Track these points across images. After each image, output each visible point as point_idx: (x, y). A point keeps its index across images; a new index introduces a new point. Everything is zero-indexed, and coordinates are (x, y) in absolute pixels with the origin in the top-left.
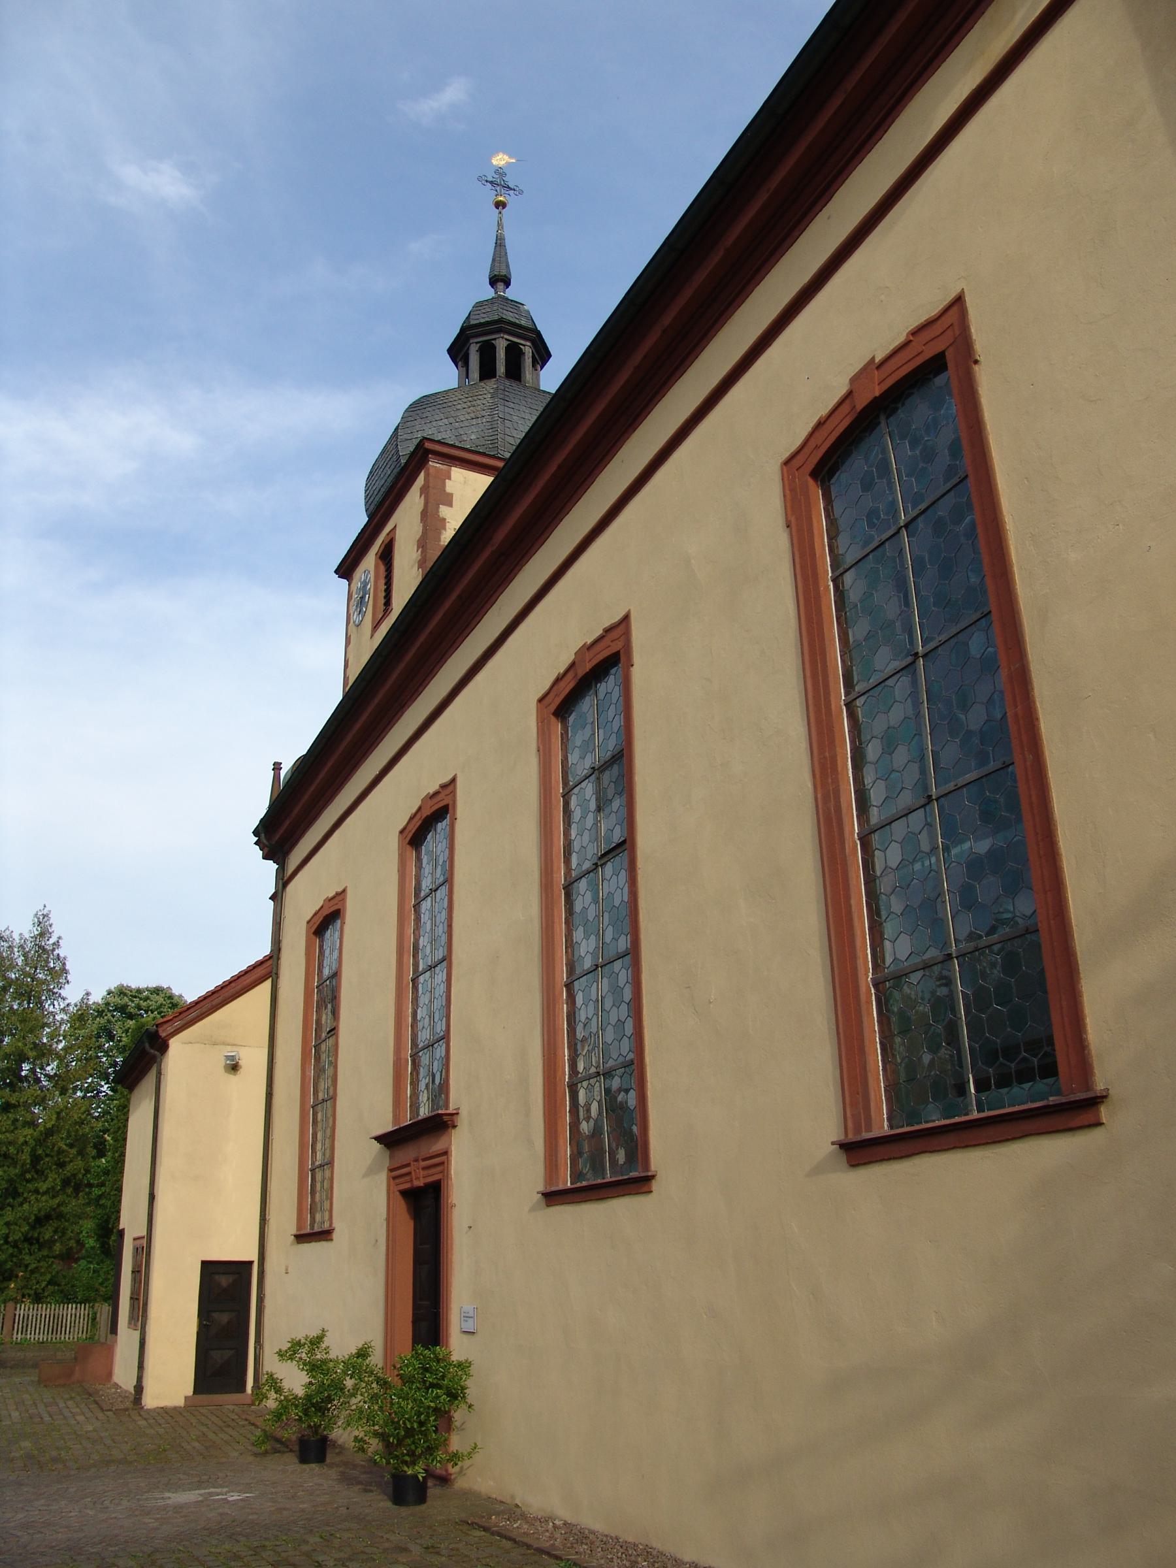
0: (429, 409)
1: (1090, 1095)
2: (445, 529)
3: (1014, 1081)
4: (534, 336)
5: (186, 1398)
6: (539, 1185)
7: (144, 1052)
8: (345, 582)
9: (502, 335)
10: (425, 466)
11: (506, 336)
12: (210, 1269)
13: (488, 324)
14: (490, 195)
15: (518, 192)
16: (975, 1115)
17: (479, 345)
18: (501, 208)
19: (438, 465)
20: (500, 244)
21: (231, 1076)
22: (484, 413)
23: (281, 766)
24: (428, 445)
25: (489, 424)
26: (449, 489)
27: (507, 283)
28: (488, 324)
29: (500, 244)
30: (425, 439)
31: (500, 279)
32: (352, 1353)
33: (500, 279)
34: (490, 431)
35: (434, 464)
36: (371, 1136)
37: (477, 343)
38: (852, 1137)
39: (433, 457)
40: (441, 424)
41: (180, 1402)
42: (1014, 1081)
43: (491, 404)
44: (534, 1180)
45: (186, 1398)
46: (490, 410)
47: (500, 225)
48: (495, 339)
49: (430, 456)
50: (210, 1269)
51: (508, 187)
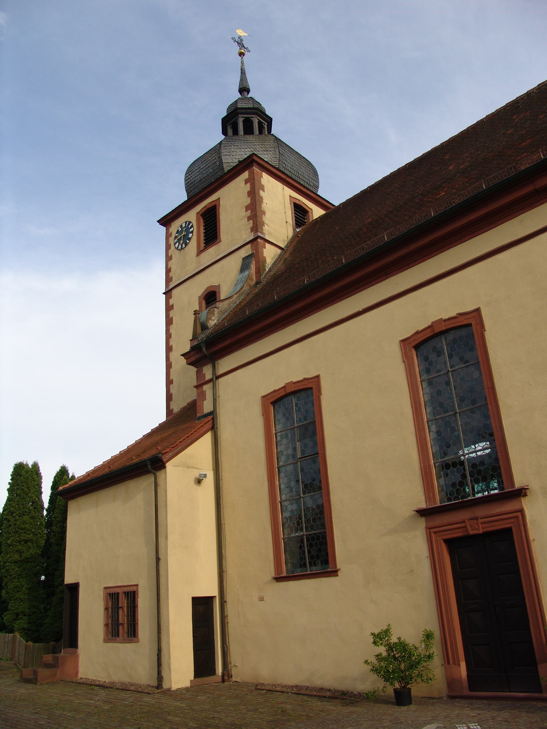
0: (238, 142)
1: (336, 569)
2: (263, 203)
3: (315, 556)
4: (269, 120)
5: (191, 681)
6: (273, 575)
7: (146, 466)
8: (164, 229)
9: (256, 116)
10: (250, 168)
11: (258, 117)
12: (196, 601)
13: (250, 109)
14: (237, 49)
15: (249, 51)
16: (309, 572)
17: (244, 118)
18: (242, 55)
19: (257, 169)
20: (243, 72)
21: (198, 487)
22: (271, 149)
23: (194, 313)
24: (255, 158)
25: (274, 155)
26: (263, 183)
27: (248, 91)
28: (250, 109)
29: (243, 72)
30: (254, 154)
31: (244, 90)
32: (376, 646)
33: (244, 90)
34: (275, 159)
35: (256, 169)
36: (413, 510)
37: (242, 117)
38: (277, 576)
39: (256, 164)
40: (246, 151)
41: (188, 684)
42: (315, 556)
43: (274, 146)
44: (271, 572)
45: (191, 681)
46: (274, 149)
47: (242, 63)
48: (252, 117)
49: (254, 164)
50: (196, 601)
51: (244, 46)
